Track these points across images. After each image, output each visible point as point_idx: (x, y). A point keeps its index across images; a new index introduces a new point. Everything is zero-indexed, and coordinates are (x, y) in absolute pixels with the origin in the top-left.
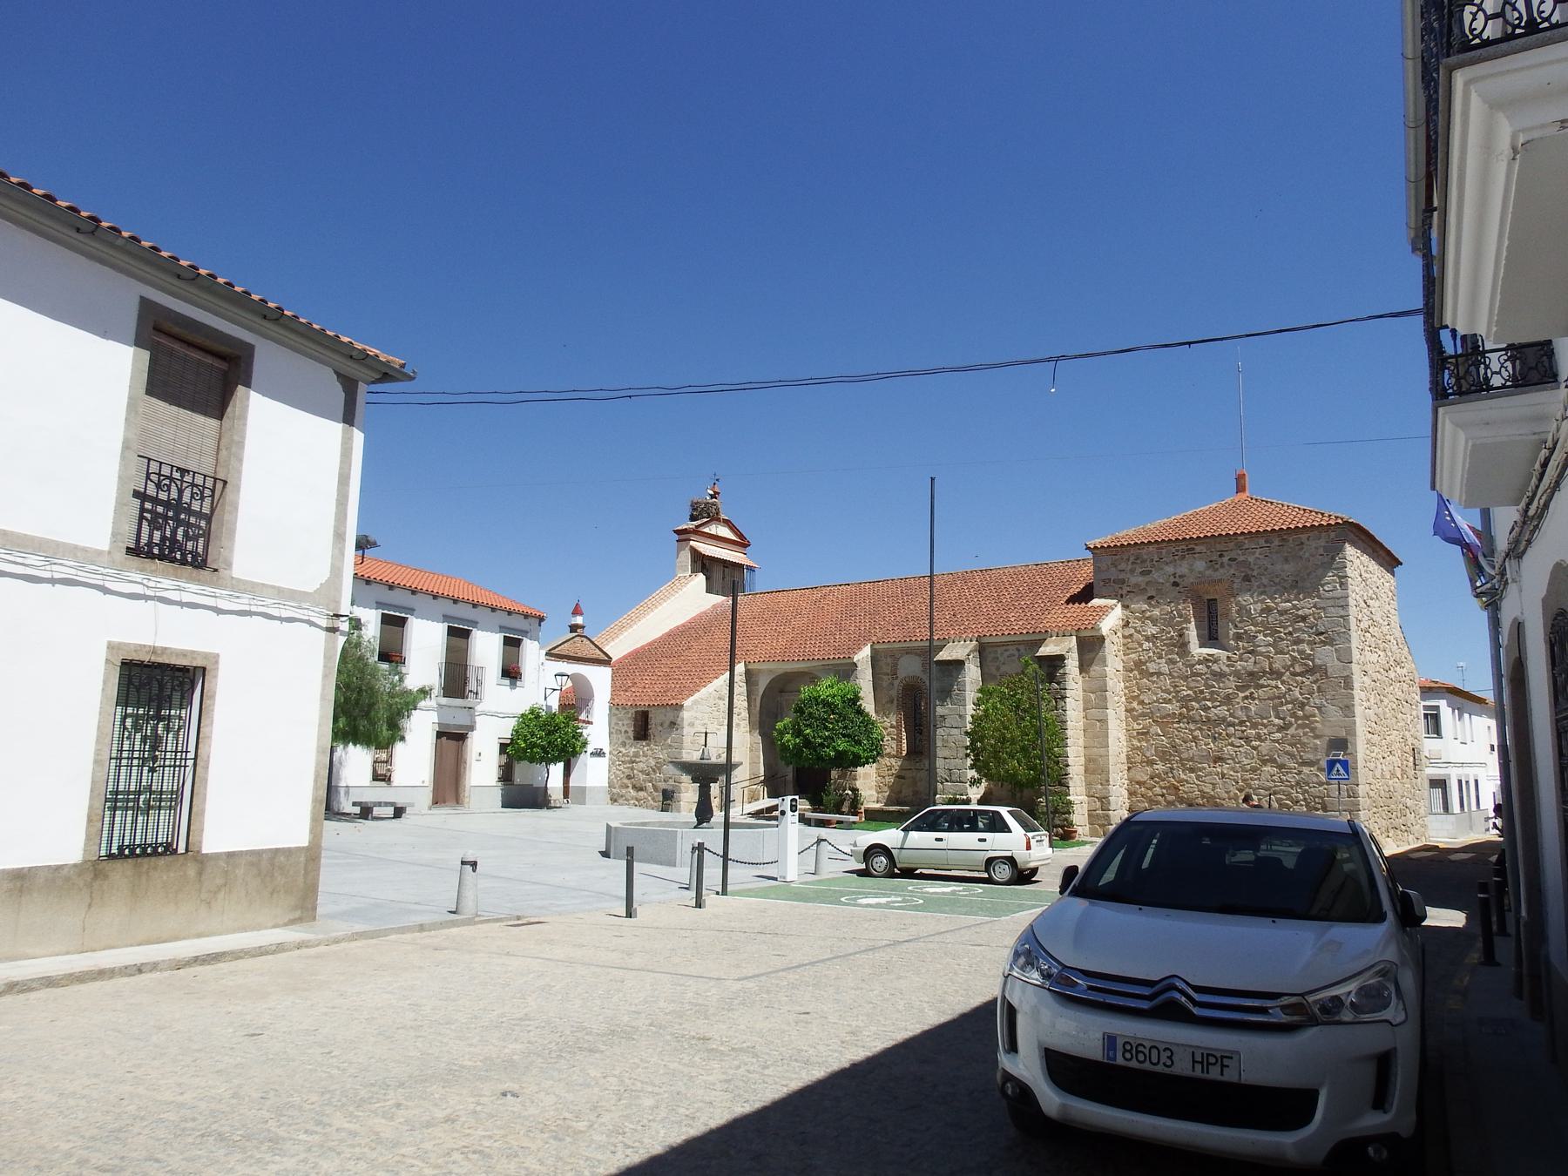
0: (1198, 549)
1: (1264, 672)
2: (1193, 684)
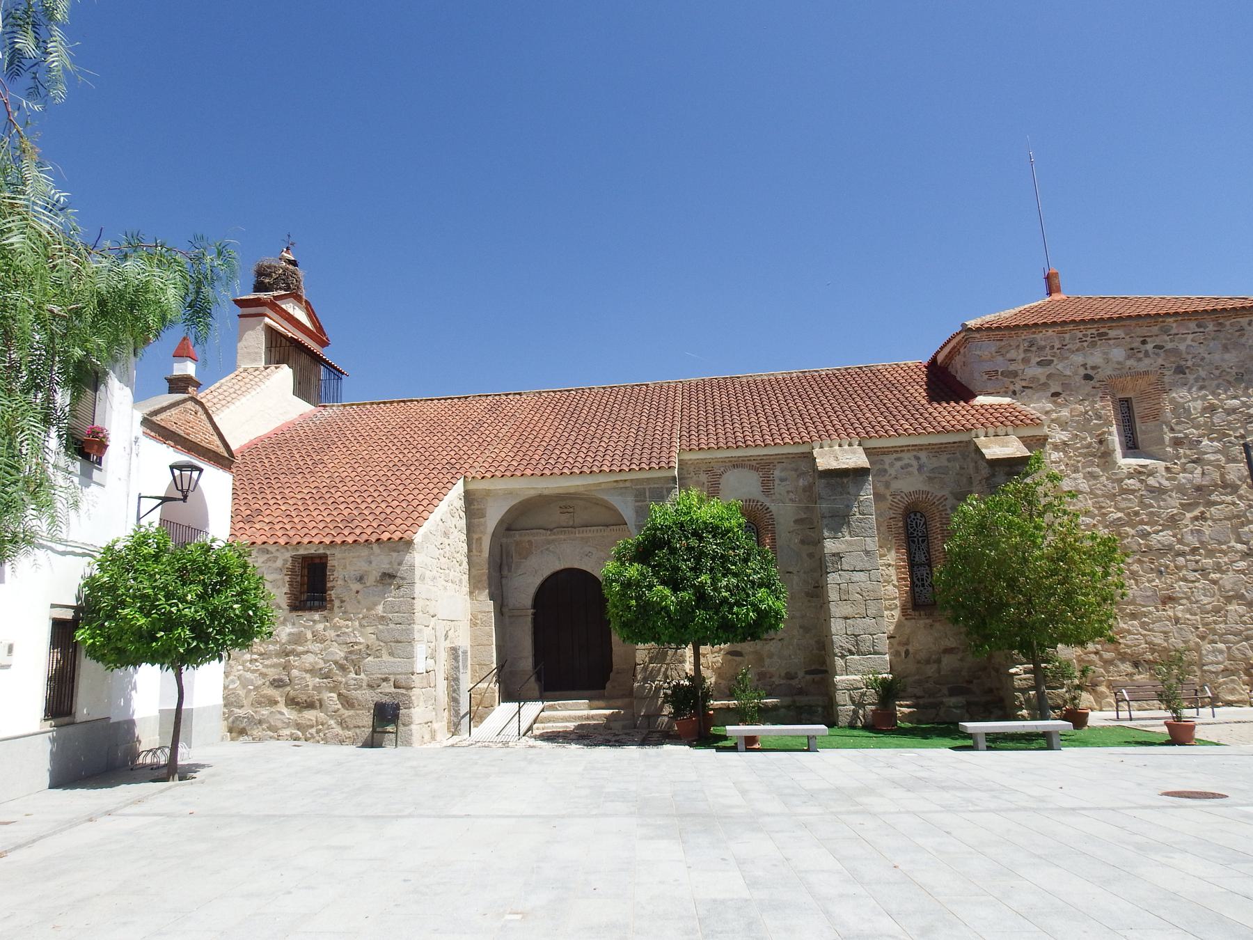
0: (1112, 333)
1: (1216, 485)
2: (1123, 505)
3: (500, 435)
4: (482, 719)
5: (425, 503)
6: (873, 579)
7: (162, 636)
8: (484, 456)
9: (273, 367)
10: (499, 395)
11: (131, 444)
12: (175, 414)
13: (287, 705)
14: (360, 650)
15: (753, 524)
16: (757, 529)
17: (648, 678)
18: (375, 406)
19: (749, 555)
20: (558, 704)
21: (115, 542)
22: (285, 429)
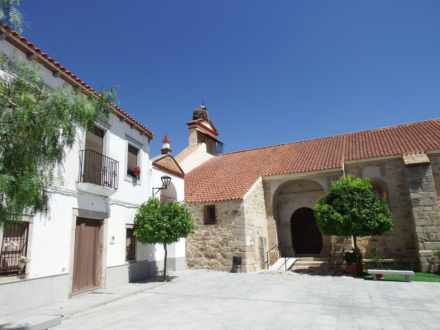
3: (276, 160)
4: (274, 263)
5: (248, 185)
6: (435, 209)
7: (157, 233)
8: (269, 168)
9: (200, 144)
10: (276, 146)
11: (149, 172)
12: (164, 161)
13: (205, 257)
14: (227, 238)
15: (378, 188)
16: (380, 190)
17: (337, 249)
18: (234, 154)
19: (374, 200)
20: (302, 259)
21: (144, 203)
22: (204, 164)
